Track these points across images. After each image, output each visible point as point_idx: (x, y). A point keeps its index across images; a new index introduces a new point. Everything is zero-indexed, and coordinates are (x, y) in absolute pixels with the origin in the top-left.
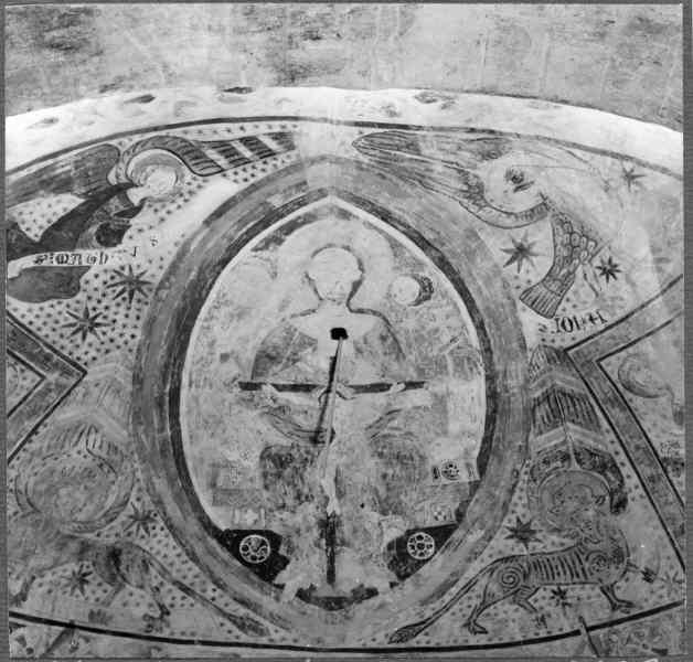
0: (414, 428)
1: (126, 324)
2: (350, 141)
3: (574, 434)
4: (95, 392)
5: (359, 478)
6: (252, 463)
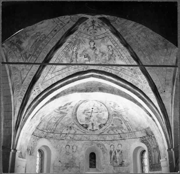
2: (76, 155)
3: (117, 117)
5: (95, 120)
6: (84, 118)
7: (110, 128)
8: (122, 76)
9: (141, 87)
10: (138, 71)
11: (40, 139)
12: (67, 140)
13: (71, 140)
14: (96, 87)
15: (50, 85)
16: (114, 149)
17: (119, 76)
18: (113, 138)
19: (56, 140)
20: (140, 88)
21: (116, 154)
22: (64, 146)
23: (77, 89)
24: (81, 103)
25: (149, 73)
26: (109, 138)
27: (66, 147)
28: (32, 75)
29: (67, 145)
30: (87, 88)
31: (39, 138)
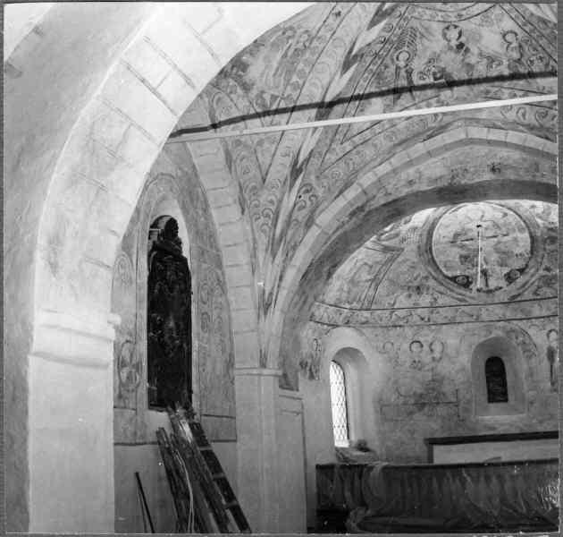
6: (457, 260)
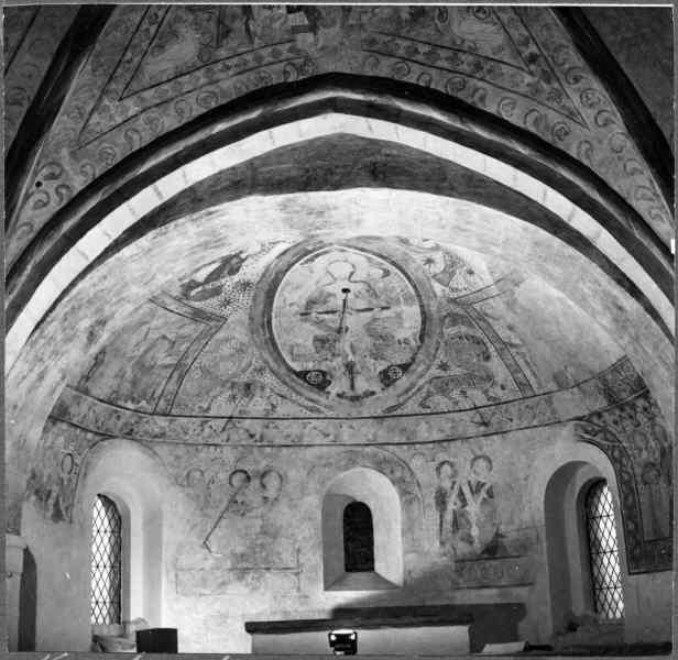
0: (386, 325)
1: (245, 300)
3: (464, 329)
4: (232, 326)
6: (310, 343)
7: (430, 382)
8: (482, 99)
9: (585, 147)
10: (563, 64)
11: (106, 443)
12: (235, 447)
13: (252, 446)
14: (355, 162)
15: (119, 158)
16: (454, 483)
17: (469, 101)
18: (448, 432)
19: (181, 451)
20: (578, 154)
21: (464, 502)
22: (223, 476)
23: (260, 177)
24: (291, 265)
25: (623, 66)
26: (430, 428)
27: (230, 478)
28: (18, 103)
29: (234, 473)
30: (308, 171)
31: (97, 438)
